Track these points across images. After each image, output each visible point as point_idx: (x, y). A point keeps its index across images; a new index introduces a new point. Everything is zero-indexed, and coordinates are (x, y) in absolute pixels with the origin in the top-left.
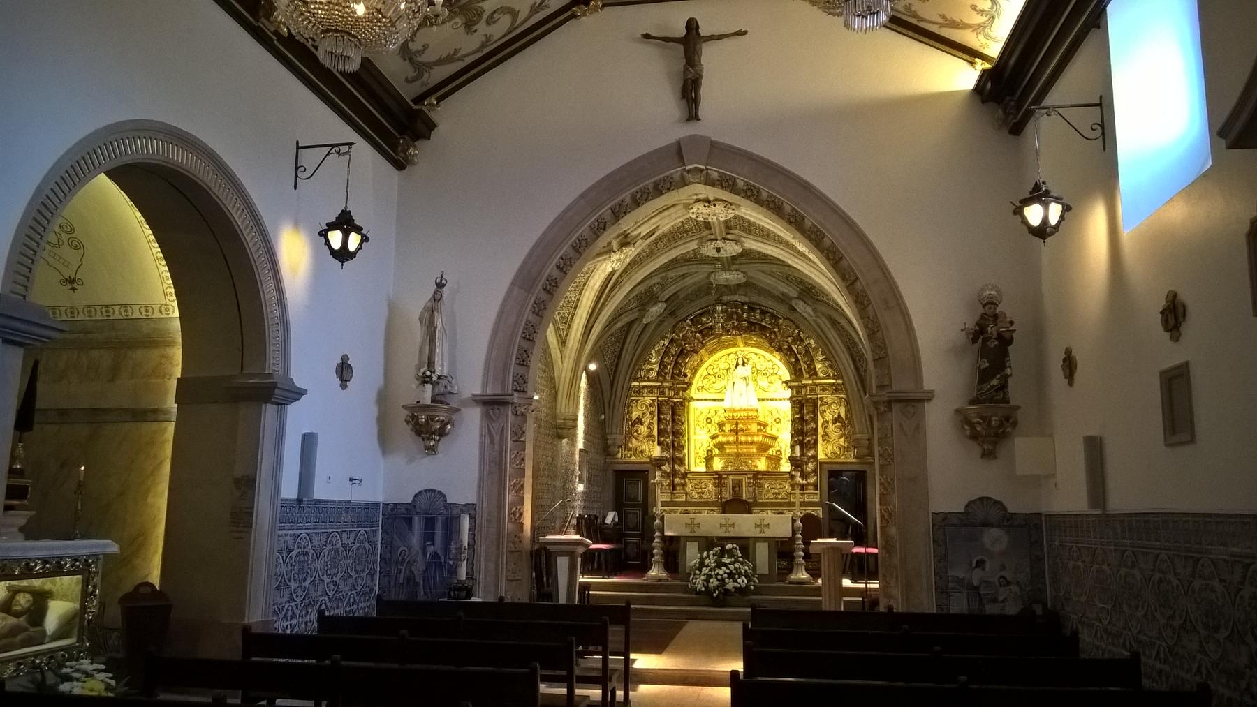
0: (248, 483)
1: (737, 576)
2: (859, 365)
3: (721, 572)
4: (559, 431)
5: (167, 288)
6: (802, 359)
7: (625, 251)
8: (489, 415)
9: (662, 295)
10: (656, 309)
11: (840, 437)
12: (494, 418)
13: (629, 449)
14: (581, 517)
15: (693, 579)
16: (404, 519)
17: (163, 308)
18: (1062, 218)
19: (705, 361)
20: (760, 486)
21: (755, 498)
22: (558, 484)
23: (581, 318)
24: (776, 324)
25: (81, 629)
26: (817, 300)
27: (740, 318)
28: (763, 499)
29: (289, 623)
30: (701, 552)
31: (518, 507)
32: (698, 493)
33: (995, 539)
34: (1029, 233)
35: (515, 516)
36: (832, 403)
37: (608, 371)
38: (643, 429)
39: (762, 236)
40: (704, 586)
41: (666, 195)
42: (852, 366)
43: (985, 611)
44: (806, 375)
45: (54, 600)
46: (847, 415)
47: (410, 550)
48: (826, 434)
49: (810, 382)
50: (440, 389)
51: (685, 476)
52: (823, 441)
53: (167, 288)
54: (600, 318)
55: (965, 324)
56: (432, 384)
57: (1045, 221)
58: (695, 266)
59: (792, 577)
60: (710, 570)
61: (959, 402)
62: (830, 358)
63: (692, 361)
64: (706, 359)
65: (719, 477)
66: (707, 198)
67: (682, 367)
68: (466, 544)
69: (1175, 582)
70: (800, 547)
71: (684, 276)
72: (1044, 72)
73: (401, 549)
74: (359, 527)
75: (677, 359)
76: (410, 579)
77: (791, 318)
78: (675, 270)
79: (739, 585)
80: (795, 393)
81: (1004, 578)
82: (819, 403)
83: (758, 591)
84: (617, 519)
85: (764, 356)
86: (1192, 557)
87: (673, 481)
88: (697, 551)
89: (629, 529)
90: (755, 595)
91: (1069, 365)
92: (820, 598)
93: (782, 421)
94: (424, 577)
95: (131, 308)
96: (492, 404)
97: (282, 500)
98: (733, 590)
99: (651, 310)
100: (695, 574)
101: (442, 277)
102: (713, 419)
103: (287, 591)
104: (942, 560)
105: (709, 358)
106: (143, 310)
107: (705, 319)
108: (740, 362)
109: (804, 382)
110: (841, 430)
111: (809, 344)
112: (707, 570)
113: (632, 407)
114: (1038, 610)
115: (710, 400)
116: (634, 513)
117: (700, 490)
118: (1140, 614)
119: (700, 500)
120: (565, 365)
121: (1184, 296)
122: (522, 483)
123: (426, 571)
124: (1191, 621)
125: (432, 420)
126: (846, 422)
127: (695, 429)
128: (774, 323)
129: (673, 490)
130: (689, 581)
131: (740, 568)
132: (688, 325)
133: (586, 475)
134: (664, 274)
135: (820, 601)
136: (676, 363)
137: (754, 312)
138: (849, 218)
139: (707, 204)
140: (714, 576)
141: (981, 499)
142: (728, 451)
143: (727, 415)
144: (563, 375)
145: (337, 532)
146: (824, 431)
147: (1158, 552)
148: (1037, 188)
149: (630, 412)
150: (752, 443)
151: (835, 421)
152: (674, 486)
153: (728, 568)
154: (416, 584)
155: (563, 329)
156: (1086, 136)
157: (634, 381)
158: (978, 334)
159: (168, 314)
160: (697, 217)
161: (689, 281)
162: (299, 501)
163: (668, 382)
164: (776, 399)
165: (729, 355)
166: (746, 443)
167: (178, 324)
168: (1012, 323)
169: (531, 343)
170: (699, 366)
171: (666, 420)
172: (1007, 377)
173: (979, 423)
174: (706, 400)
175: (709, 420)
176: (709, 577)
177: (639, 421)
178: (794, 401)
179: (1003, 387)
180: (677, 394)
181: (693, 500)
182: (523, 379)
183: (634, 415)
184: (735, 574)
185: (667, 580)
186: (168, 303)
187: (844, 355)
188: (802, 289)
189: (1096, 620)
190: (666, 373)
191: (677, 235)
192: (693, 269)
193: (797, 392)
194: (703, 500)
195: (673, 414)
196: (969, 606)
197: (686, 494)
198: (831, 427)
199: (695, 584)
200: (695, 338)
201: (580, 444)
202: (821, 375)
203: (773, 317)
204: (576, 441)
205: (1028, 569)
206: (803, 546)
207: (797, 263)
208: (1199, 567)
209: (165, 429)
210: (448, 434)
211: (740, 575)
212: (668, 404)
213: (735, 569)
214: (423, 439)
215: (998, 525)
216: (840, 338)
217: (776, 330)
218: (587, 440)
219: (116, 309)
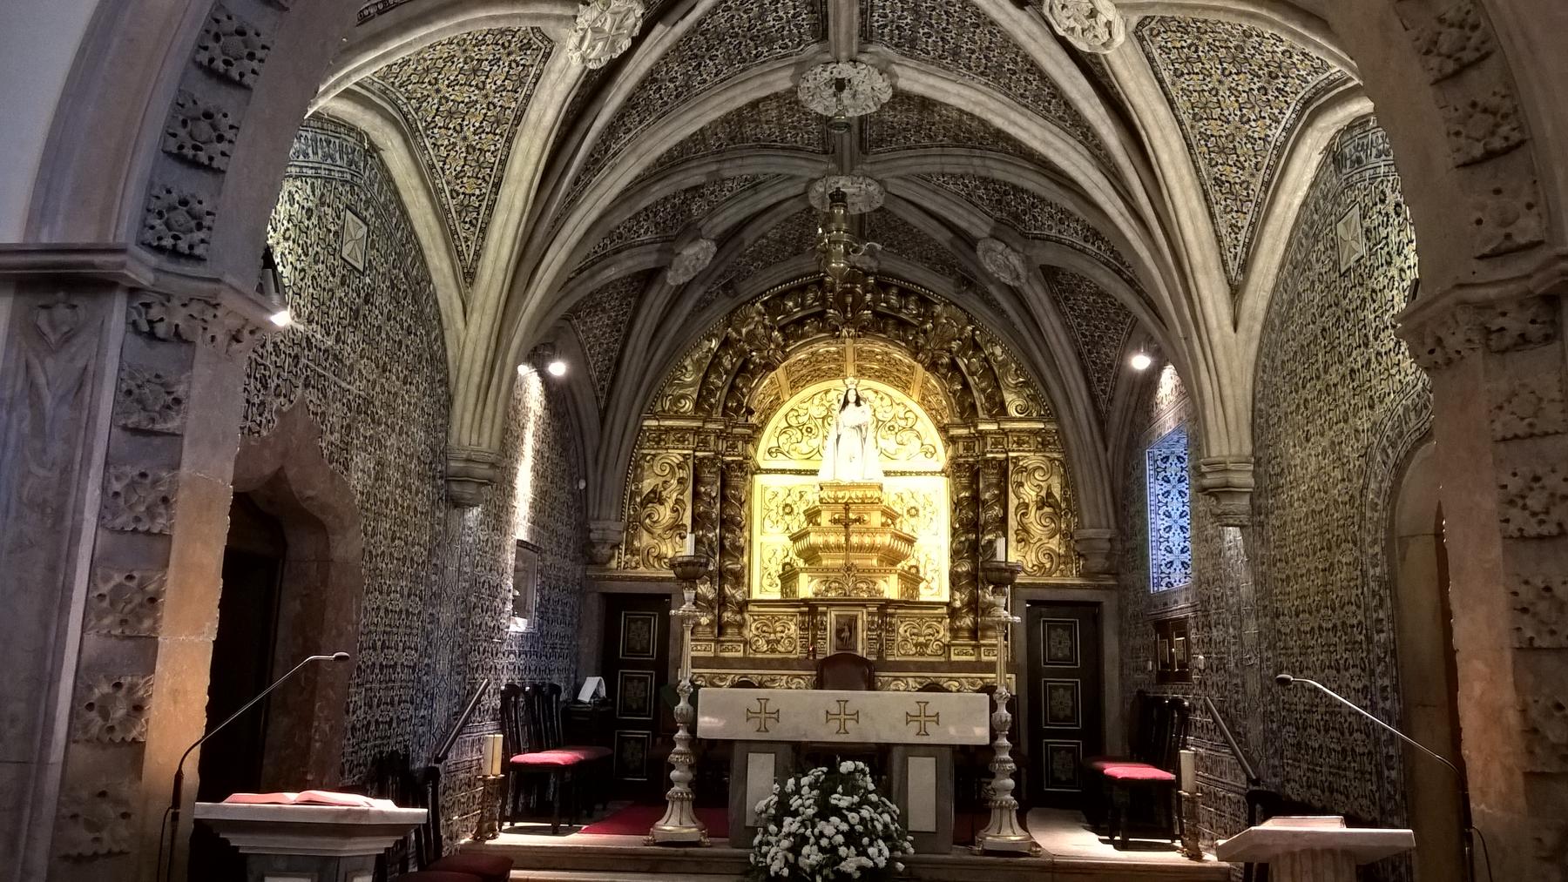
1: (866, 840)
2: (1098, 389)
3: (829, 830)
4: (455, 488)
8: (37, 327)
9: (710, 225)
10: (696, 255)
12: (53, 338)
13: (633, 551)
14: (512, 690)
15: (761, 844)
20: (891, 629)
21: (880, 652)
22: (447, 615)
23: (510, 211)
26: (1035, 238)
27: (858, 303)
28: (895, 656)
30: (780, 778)
32: (768, 642)
36: (1035, 469)
37: (595, 391)
38: (664, 514)
40: (787, 864)
42: (1084, 393)
48: (1024, 529)
49: (994, 427)
51: (743, 606)
52: (1019, 541)
58: (780, 160)
60: (803, 823)
64: (787, 397)
65: (811, 608)
67: (744, 396)
75: (734, 380)
79: (871, 864)
82: (1011, 467)
84: (603, 692)
87: (720, 617)
88: (772, 777)
89: (628, 710)
93: (921, 512)
98: (857, 875)
99: (685, 253)
100: (766, 831)
102: (795, 507)
105: (791, 396)
107: (791, 304)
108: (852, 398)
110: (1053, 521)
111: (993, 354)
113: (643, 469)
115: (791, 472)
116: (640, 680)
117: (772, 637)
120: (473, 328)
126: (1063, 505)
127: (762, 524)
128: (924, 316)
129: (720, 634)
132: (759, 313)
133: (534, 599)
134: (714, 167)
136: (733, 388)
137: (887, 294)
140: (812, 840)
142: (824, 562)
143: (824, 494)
144: (468, 353)
146: (1020, 523)
149: (638, 479)
150: (873, 548)
151: (1041, 505)
152: (721, 627)
153: (844, 819)
155: (467, 239)
157: (649, 418)
164: (911, 473)
165: (827, 392)
166: (861, 548)
171: (710, 495)
174: (783, 471)
175: (788, 509)
177: (656, 497)
178: (959, 465)
180: (733, 447)
181: (759, 656)
183: (647, 485)
184: (861, 835)
188: (997, 220)
190: (711, 406)
193: (966, 449)
194: (777, 656)
195: (724, 485)
197: (746, 643)
198: (1033, 514)
199: (765, 856)
200: (770, 339)
201: (521, 526)
202: (1012, 412)
203: (924, 301)
204: (508, 522)
206: (1013, 765)
207: (1015, 123)
213: (862, 820)
217: (929, 326)
218: (536, 522)
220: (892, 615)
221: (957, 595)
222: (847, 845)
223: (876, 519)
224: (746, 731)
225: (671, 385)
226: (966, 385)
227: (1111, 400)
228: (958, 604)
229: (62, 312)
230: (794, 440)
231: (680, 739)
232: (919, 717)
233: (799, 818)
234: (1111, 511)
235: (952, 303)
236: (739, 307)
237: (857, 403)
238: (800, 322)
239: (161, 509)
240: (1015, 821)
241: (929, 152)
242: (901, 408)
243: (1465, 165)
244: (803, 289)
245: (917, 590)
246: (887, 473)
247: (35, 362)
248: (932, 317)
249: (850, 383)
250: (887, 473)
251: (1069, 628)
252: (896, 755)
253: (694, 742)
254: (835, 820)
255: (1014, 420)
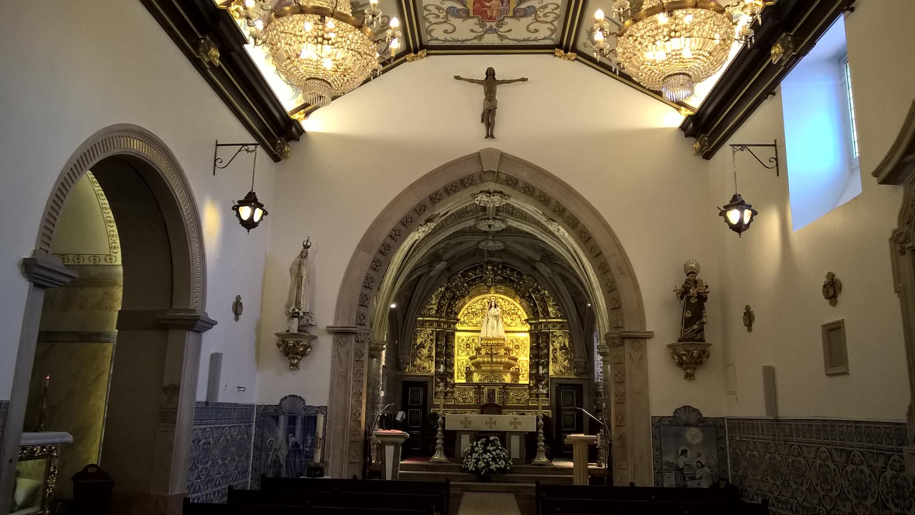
0: (175, 390)
1: (498, 460)
3: (487, 457)
5: (112, 243)
6: (539, 304)
7: (429, 225)
8: (339, 342)
10: (441, 266)
11: (565, 361)
12: (342, 343)
13: (414, 366)
14: (383, 416)
15: (466, 462)
16: (273, 417)
17: (108, 258)
18: (751, 219)
19: (466, 303)
20: (508, 394)
21: (503, 403)
24: (521, 279)
25: (44, 501)
26: (555, 263)
29: (197, 495)
30: (471, 442)
31: (358, 409)
33: (693, 435)
34: (730, 228)
35: (355, 415)
38: (425, 352)
39: (521, 218)
40: (474, 467)
41: (469, 188)
43: (687, 486)
44: (541, 316)
45: (20, 478)
46: (570, 345)
47: (276, 440)
48: (555, 358)
49: (545, 320)
50: (304, 322)
52: (553, 362)
53: (112, 243)
54: (405, 270)
55: (676, 286)
56: (299, 318)
57: (741, 221)
59: (536, 461)
60: (479, 455)
61: (673, 340)
62: (559, 304)
63: (459, 303)
65: (478, 387)
66: (489, 190)
68: (321, 436)
69: (832, 466)
70: (542, 438)
71: (460, 243)
72: (729, 124)
73: (270, 439)
74: (241, 423)
75: (450, 302)
76: (276, 462)
77: (531, 274)
78: (455, 239)
80: (533, 329)
81: (699, 462)
82: (551, 335)
83: (512, 471)
84: (404, 417)
85: (508, 301)
86: (846, 450)
90: (511, 473)
91: (749, 317)
92: (572, 476)
93: (520, 347)
94: (286, 460)
95: (82, 257)
96: (340, 333)
97: (197, 403)
99: (436, 266)
100: (468, 458)
101: (308, 241)
103: (196, 471)
104: (658, 450)
105: (469, 301)
106: (92, 258)
107: (471, 274)
108: (493, 305)
109: (540, 321)
111: (544, 293)
112: (477, 455)
114: (722, 485)
118: (804, 488)
119: (464, 404)
120: (379, 304)
121: (839, 276)
122: (361, 391)
123: (288, 456)
124: (844, 493)
125: (298, 344)
127: (458, 352)
130: (463, 463)
131: (500, 454)
132: (459, 278)
133: (385, 384)
135: (572, 478)
136: (450, 304)
138: (596, 210)
139: (488, 195)
140: (482, 460)
141: (684, 407)
142: (483, 368)
145: (228, 426)
146: (554, 356)
147: (819, 446)
148: (735, 198)
150: (501, 363)
151: (561, 349)
153: (491, 454)
154: (280, 466)
156: (766, 166)
158: (684, 293)
159: (111, 262)
160: (480, 203)
161: (464, 246)
162: (207, 403)
163: (444, 318)
165: (483, 299)
166: (497, 363)
167: (120, 270)
168: (707, 287)
169: (370, 290)
170: (462, 306)
171: (441, 345)
172: (704, 323)
173: (684, 355)
175: (468, 346)
176: (478, 460)
177: (422, 346)
178: (532, 334)
179: (701, 330)
180: (450, 326)
182: (363, 316)
183: (419, 341)
184: (497, 458)
185: (446, 463)
186: (112, 254)
187: (570, 302)
188: (543, 255)
189: (769, 492)
191: (461, 214)
192: (468, 238)
194: (466, 404)
195: (447, 341)
196: (676, 482)
198: (558, 353)
199: (467, 465)
200: (463, 287)
201: (383, 363)
203: (519, 273)
205: (716, 457)
208: (851, 457)
209: (105, 349)
210: (307, 355)
211: (500, 458)
212: (443, 334)
213: (497, 454)
214: (289, 359)
215: (696, 426)
216: (568, 291)
219: (71, 257)
220: (508, 389)
221: (531, 382)
222: (492, 461)
223: (502, 352)
224: (461, 428)
225: (427, 304)
226: (535, 303)
227: (584, 313)
228: (532, 385)
229: (344, 339)
230: (470, 318)
231: (440, 430)
232: (515, 423)
233: (477, 454)
234: (585, 351)
235: (530, 275)
236: (452, 275)
237: (495, 307)
238: (474, 280)
239: (361, 376)
240: (544, 455)
241: (519, 235)
242: (512, 306)
243: (612, 309)
244: (475, 269)
245: (519, 378)
246: (507, 332)
247: (339, 348)
248: (523, 280)
249: (492, 296)
250: (507, 332)
251: (571, 393)
252: (507, 435)
253: (445, 432)
254: (488, 454)
255: (551, 318)
